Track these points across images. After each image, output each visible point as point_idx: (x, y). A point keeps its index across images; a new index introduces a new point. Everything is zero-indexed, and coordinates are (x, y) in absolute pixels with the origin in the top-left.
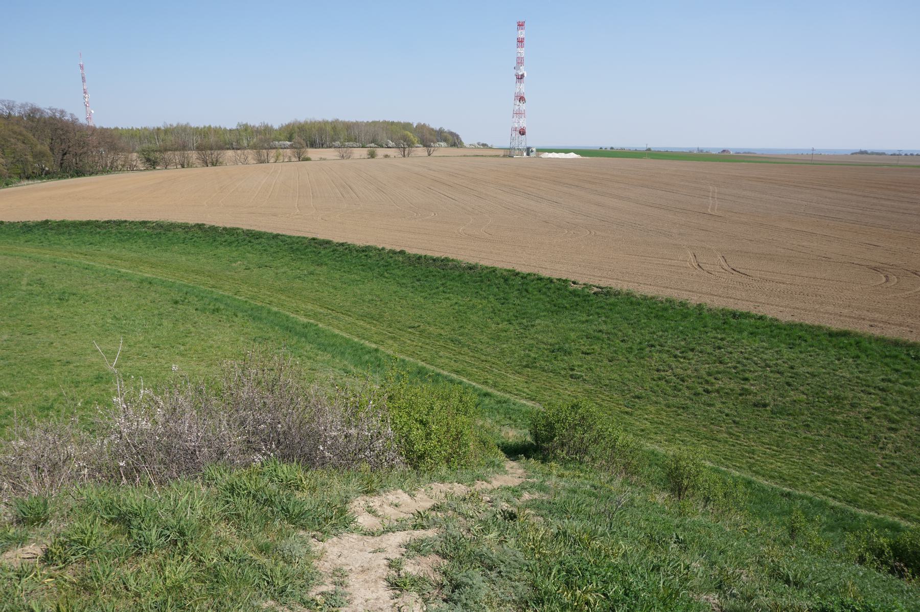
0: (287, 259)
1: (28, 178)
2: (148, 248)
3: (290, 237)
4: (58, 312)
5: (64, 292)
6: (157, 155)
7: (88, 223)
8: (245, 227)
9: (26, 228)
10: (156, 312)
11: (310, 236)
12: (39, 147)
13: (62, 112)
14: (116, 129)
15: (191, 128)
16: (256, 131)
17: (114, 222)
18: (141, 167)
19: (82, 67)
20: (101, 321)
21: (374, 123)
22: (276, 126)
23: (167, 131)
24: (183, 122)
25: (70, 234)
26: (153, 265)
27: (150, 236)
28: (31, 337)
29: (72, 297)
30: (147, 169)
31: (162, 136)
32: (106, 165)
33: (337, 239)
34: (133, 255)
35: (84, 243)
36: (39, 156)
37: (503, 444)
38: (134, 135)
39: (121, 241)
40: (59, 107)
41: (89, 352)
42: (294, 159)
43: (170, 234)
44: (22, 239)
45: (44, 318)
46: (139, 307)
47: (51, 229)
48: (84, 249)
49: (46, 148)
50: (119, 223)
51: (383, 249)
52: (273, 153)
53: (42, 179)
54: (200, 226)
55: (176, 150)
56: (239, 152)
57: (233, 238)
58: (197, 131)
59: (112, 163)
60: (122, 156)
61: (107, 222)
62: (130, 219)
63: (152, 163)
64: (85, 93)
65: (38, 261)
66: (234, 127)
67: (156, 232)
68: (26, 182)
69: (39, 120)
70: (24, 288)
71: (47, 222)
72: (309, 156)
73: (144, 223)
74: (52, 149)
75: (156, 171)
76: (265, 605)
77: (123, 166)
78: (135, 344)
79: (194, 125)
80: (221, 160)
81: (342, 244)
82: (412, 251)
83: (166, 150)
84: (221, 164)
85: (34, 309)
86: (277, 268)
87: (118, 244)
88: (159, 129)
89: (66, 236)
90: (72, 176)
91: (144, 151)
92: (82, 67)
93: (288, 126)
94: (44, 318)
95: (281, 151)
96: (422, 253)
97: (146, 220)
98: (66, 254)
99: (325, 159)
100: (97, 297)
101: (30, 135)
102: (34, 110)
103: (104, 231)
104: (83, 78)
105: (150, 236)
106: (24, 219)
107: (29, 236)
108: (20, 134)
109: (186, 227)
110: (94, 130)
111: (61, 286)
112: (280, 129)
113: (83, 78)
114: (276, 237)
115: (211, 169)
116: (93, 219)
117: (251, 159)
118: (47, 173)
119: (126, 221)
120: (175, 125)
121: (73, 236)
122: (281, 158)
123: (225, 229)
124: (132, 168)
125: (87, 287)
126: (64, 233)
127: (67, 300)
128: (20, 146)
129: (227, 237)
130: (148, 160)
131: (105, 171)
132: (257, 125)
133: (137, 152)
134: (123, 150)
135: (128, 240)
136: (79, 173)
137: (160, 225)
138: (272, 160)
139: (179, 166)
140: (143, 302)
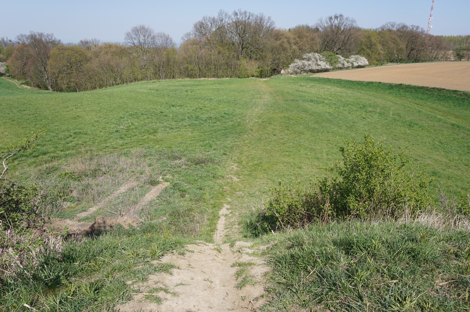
1: (391, 62)
2: (455, 106)
4: (408, 132)
5: (411, 122)
6: (465, 52)
7: (422, 88)
10: (466, 145)
12: (401, 46)
13: (418, 27)
17: (437, 89)
18: (452, 58)
20: (432, 142)
25: (411, 92)
26: (456, 117)
27: (458, 99)
28: (396, 141)
29: (415, 126)
30: (456, 60)
32: (432, 57)
35: (418, 98)
36: (399, 50)
37: (130, 299)
38: (451, 40)
39: (439, 100)
40: (416, 25)
41: (426, 157)
44: (388, 92)
45: (402, 133)
46: (454, 139)
47: (403, 89)
48: (417, 101)
50: (440, 90)
53: (398, 63)
59: (436, 56)
60: (443, 52)
61: (433, 88)
63: (459, 57)
64: (431, 16)
65: (396, 104)
67: (461, 97)
68: (390, 64)
69: (405, 31)
70: (391, 116)
71: (401, 84)
73: (455, 91)
74: (407, 47)
75: (461, 62)
76: (149, 308)
77: (442, 58)
78: (453, 160)
85: (397, 128)
87: (437, 101)
89: (409, 93)
90: (413, 62)
91: (457, 49)
94: (402, 133)
97: (457, 90)
98: (408, 102)
100: (429, 128)
102: (404, 27)
103: (430, 93)
104: (432, 8)
106: (390, 82)
107: (391, 91)
110: (431, 37)
111: (409, 119)
113: (432, 8)
116: (426, 85)
119: (444, 89)
121: (413, 94)
124: (447, 59)
125: (423, 122)
126: (408, 92)
127: (413, 127)
130: (458, 55)
131: (431, 60)
133: (453, 50)
135: (443, 100)
136: (417, 60)
140: (456, 137)
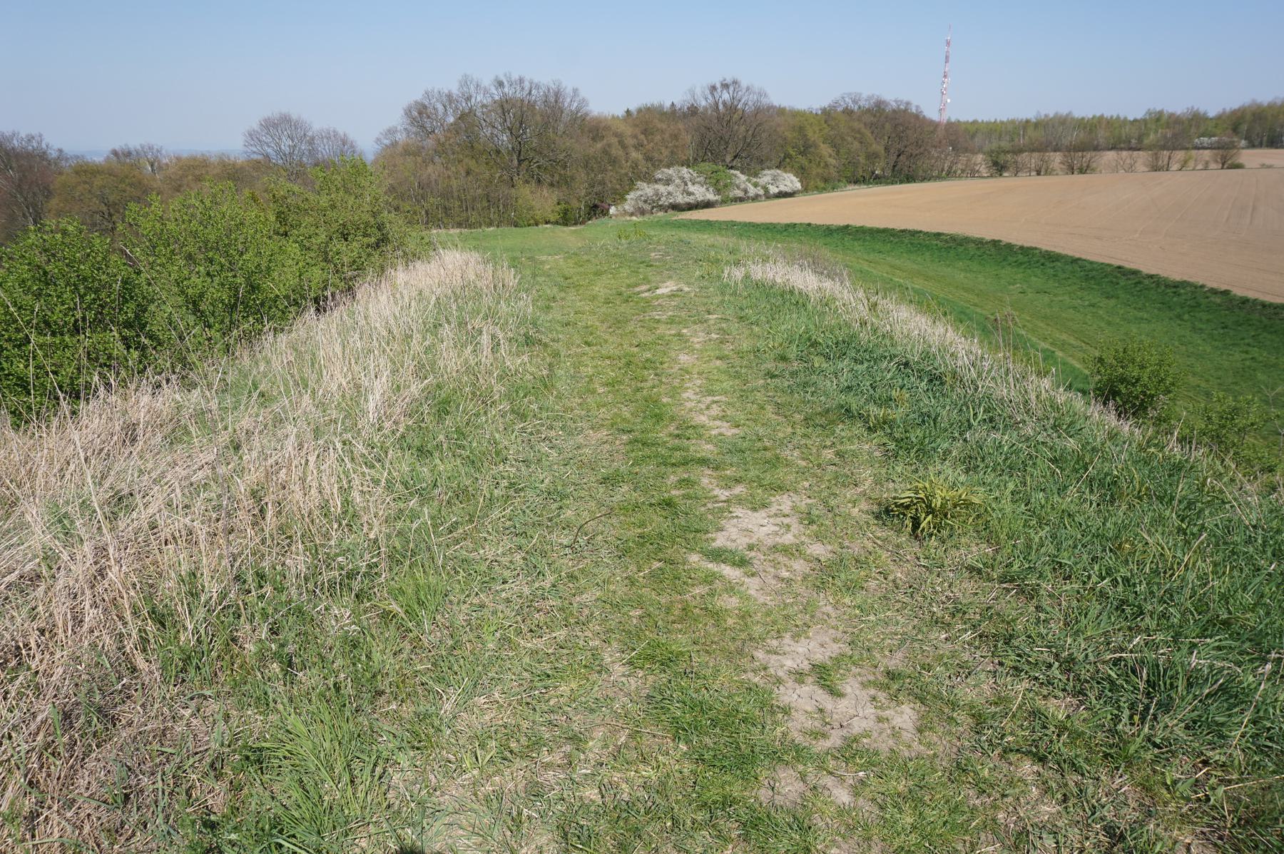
0: (1075, 287)
1: (856, 182)
3: (1091, 263)
7: (885, 231)
8: (1044, 248)
9: (829, 232)
11: (1116, 263)
14: (975, 122)
15: (1073, 119)
16: (1174, 121)
19: (948, 43)
21: (1013, 122)
22: (1212, 114)
23: (1037, 125)
24: (1063, 111)
26: (927, 278)
27: (940, 249)
30: (991, 176)
31: (1030, 132)
33: (1146, 269)
34: (915, 266)
36: (872, 157)
42: (1213, 166)
43: (961, 249)
48: (872, 257)
49: (881, 149)
50: (914, 233)
51: (1203, 286)
52: (1180, 155)
53: (869, 183)
54: (995, 243)
55: (1033, 151)
56: (1125, 153)
57: (1026, 259)
58: (1082, 124)
59: (950, 167)
62: (925, 229)
63: (999, 168)
66: (1139, 116)
72: (1241, 161)
73: (939, 234)
77: (963, 171)
79: (1078, 114)
80: (1094, 165)
81: (1151, 276)
82: (1238, 292)
83: (1021, 151)
84: (1093, 170)
86: (1055, 295)
88: (1028, 121)
89: (860, 242)
90: (901, 182)
92: (948, 43)
93: (1234, 112)
95: (1194, 152)
96: (1251, 295)
99: (1270, 167)
101: (868, 133)
104: (947, 57)
105: (940, 249)
107: (828, 240)
108: (859, 132)
109: (980, 243)
112: (1219, 117)
113: (947, 57)
114: (1075, 261)
115: (1078, 178)
117: (1140, 167)
118: (877, 177)
120: (1051, 116)
122: (1191, 164)
123: (1022, 248)
128: (856, 145)
129: (1020, 256)
132: (1179, 112)
134: (966, 150)
137: (953, 238)
138: (1175, 167)
139: (1034, 173)
